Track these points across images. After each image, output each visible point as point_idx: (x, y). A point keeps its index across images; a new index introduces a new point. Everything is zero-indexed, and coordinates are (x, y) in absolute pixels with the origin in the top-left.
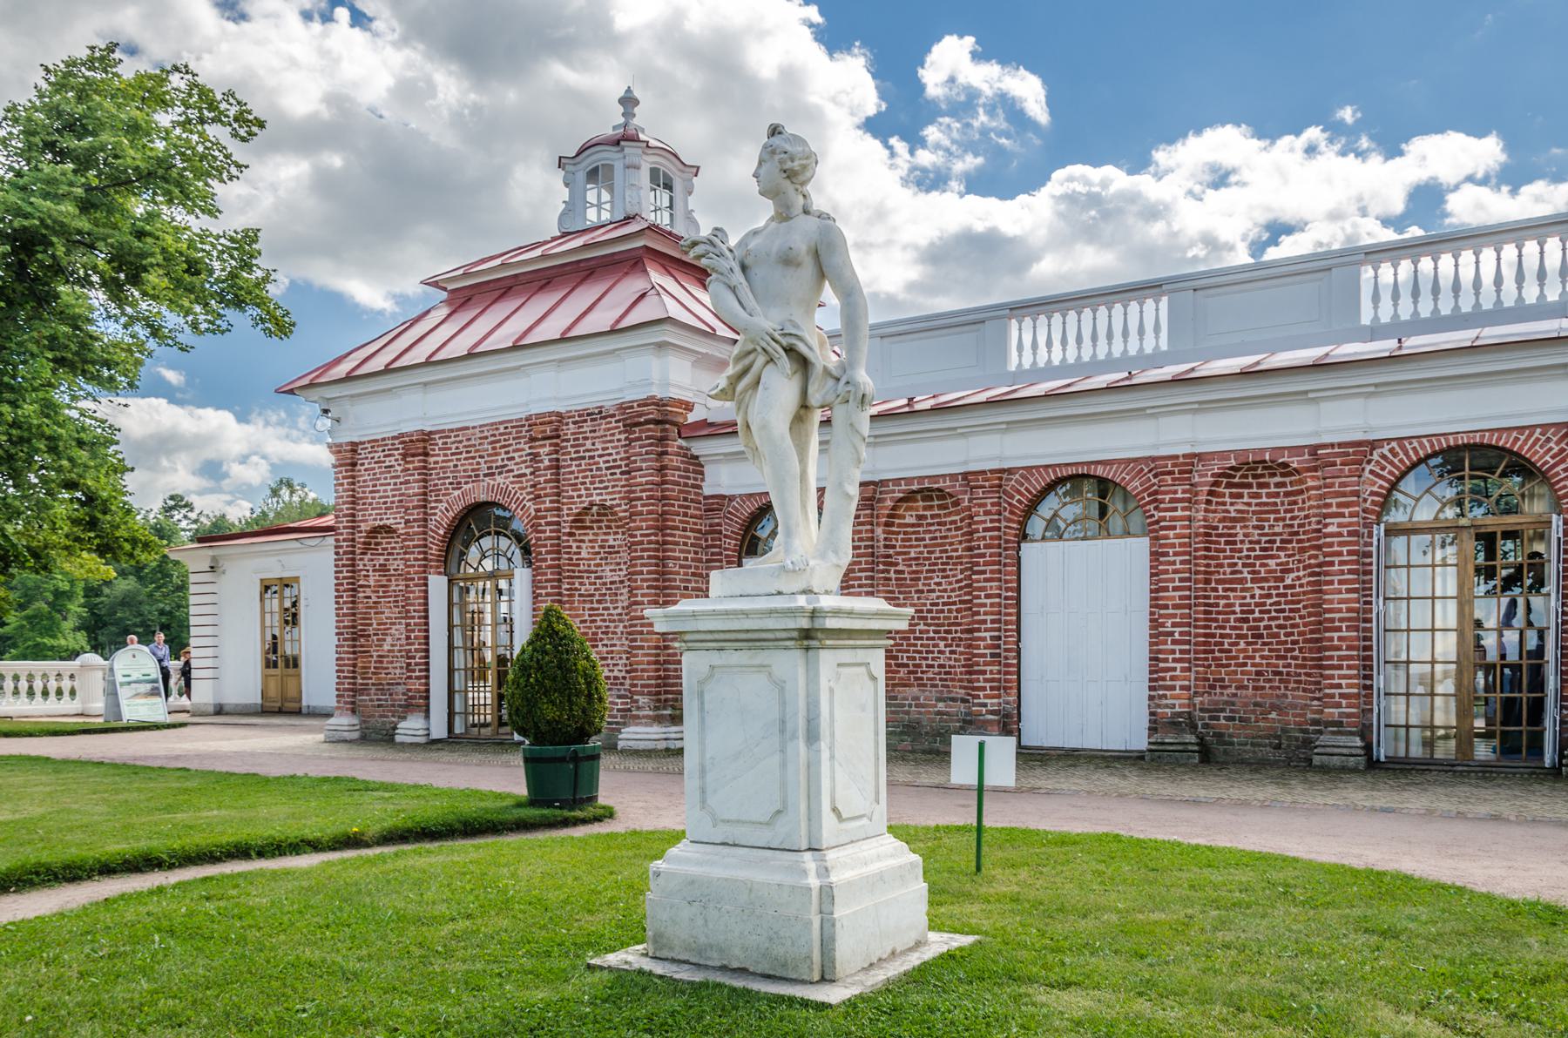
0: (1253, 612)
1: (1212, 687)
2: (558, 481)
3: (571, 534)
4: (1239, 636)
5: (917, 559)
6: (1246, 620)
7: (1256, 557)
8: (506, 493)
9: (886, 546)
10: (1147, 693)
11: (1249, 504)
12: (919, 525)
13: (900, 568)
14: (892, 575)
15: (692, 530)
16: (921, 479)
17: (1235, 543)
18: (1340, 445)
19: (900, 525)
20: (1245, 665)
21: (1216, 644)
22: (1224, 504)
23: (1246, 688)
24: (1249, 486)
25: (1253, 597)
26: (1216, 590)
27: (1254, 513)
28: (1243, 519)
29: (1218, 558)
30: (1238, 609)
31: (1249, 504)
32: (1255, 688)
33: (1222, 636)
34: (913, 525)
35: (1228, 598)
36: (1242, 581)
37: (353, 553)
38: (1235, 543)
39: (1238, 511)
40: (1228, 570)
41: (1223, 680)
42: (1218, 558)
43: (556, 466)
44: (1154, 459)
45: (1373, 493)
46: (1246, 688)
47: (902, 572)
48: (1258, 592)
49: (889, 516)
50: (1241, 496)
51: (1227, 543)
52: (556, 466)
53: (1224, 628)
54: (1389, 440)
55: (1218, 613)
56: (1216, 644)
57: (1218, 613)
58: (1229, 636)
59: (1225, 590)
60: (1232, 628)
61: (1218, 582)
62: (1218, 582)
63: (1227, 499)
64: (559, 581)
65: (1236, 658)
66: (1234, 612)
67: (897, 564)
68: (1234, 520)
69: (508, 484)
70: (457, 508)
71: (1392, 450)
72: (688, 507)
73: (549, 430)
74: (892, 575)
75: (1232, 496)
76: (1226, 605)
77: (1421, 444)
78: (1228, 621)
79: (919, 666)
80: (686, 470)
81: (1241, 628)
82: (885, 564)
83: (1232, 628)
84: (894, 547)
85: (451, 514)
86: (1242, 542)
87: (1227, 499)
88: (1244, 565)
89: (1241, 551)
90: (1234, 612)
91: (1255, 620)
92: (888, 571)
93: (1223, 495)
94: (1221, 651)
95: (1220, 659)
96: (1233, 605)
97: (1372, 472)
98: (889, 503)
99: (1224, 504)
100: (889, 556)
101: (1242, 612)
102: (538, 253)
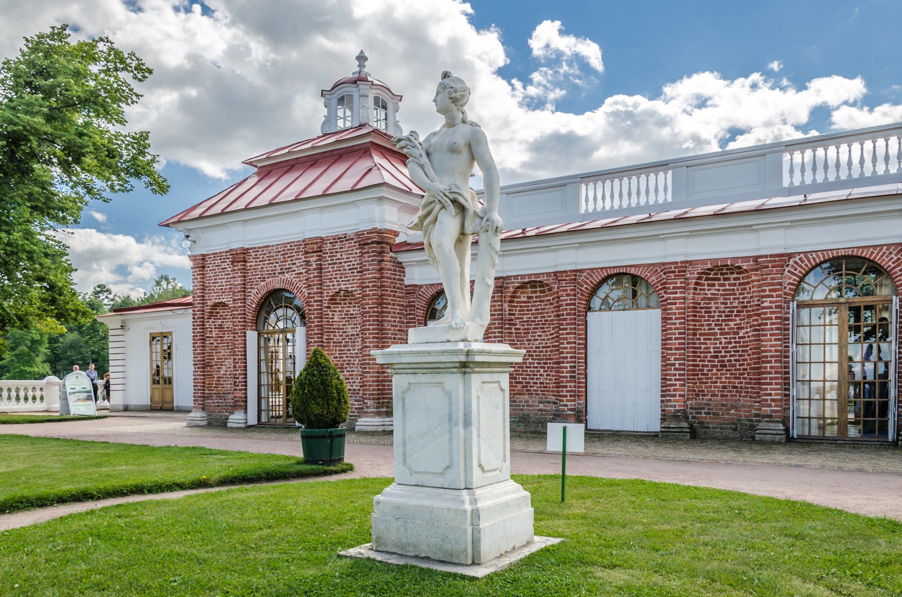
0: (721, 352)
1: (697, 395)
2: (321, 277)
3: (328, 307)
4: (713, 366)
5: (527, 321)
6: (717, 357)
7: (723, 321)
8: (291, 283)
9: (510, 314)
10: (660, 398)
11: (719, 290)
12: (529, 302)
13: (518, 327)
14: (513, 331)
15: (398, 305)
16: (530, 275)
17: (710, 312)
18: (771, 256)
19: (518, 302)
20: (716, 382)
21: (699, 370)
22: (704, 290)
23: (717, 395)
24: (719, 279)
25: (721, 343)
26: (699, 339)
27: (721, 295)
28: (715, 299)
29: (700, 321)
30: (712, 350)
31: (719, 290)
32: (722, 396)
33: (703, 366)
34: (525, 302)
35: (706, 344)
36: (715, 334)
37: (203, 318)
38: (710, 312)
39: (712, 294)
40: (707, 328)
41: (703, 391)
42: (700, 321)
43: (320, 268)
44: (664, 264)
45: (790, 284)
46: (717, 395)
47: (519, 329)
48: (723, 340)
49: (512, 297)
50: (714, 285)
51: (706, 312)
52: (320, 268)
53: (704, 361)
54: (799, 253)
55: (701, 352)
56: (699, 370)
57: (701, 352)
58: (707, 366)
59: (705, 339)
60: (709, 361)
61: (701, 335)
62: (701, 335)
63: (706, 287)
64: (322, 334)
65: (711, 378)
66: (710, 352)
67: (516, 325)
68: (710, 299)
69: (292, 278)
70: (263, 292)
71: (801, 259)
72: (396, 292)
73: (316, 247)
74: (513, 331)
75: (709, 285)
76: (705, 348)
77: (818, 255)
78: (706, 357)
79: (529, 383)
80: (395, 270)
81: (714, 361)
82: (509, 324)
83: (709, 361)
84: (514, 314)
85: (259, 296)
86: (715, 312)
87: (706, 287)
88: (716, 325)
89: (714, 317)
90: (710, 352)
91: (722, 357)
92: (511, 329)
93: (704, 285)
94: (702, 374)
95: (702, 379)
96: (709, 348)
97: (789, 271)
98: (512, 289)
99: (704, 290)
100: (512, 320)
101: (715, 352)
102: (309, 145)
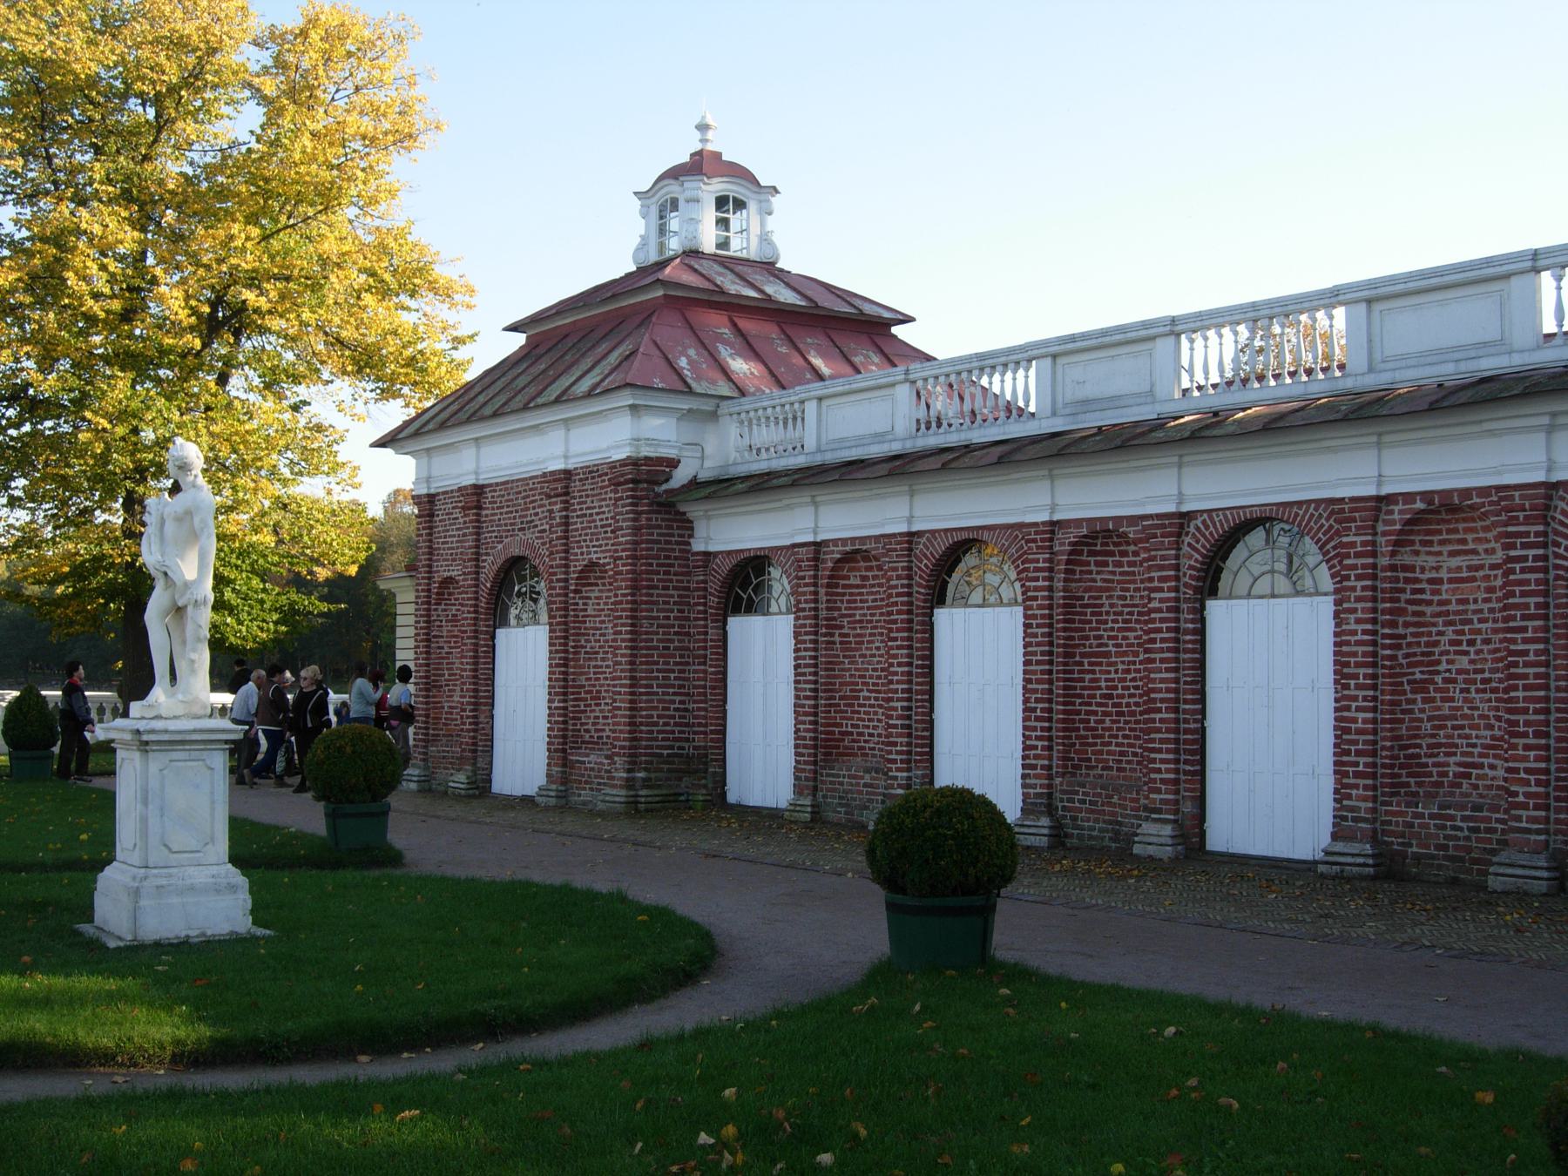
0: (1116, 688)
1: (1077, 767)
2: (567, 538)
3: (576, 592)
4: (1105, 714)
5: (861, 621)
6: (1110, 697)
7: (1119, 630)
8: (533, 548)
9: (828, 609)
10: (1020, 771)
11: (1113, 573)
12: (864, 586)
13: (845, 631)
14: (837, 639)
15: (675, 588)
16: (853, 540)
17: (1100, 614)
18: (1159, 516)
19: (845, 586)
20: (1110, 744)
21: (1081, 721)
22: (1090, 572)
23: (1111, 768)
24: (1112, 554)
25: (1116, 672)
26: (1081, 664)
27: (1119, 582)
28: (1108, 589)
29: (1083, 630)
30: (1103, 684)
31: (1113, 573)
32: (1119, 769)
33: (1088, 713)
34: (857, 586)
35: (1093, 672)
36: (1107, 655)
37: (429, 603)
38: (1100, 614)
39: (1104, 580)
40: (1095, 642)
41: (1089, 760)
42: (1083, 630)
43: (566, 523)
44: (1499, 488)
45: (1191, 567)
46: (1111, 768)
47: (847, 635)
48: (1121, 667)
49: (830, 577)
50: (1106, 564)
51: (1093, 614)
52: (566, 523)
53: (1090, 704)
54: (1203, 512)
55: (1083, 688)
56: (1081, 721)
57: (1083, 688)
58: (1095, 713)
59: (1090, 664)
60: (1099, 705)
61: (1083, 655)
62: (1083, 655)
63: (1093, 568)
64: (566, 638)
65: (1102, 736)
66: (1100, 688)
67: (842, 627)
68: (1101, 589)
69: (529, 538)
70: (500, 562)
71: (1204, 522)
72: (672, 565)
73: (562, 483)
74: (837, 639)
75: (1097, 564)
76: (1092, 680)
77: (1225, 516)
78: (1094, 696)
79: (862, 734)
80: (668, 527)
81: (1106, 705)
82: (827, 627)
83: (1099, 705)
84: (839, 609)
85: (495, 567)
86: (1108, 613)
87: (1093, 568)
88: (1110, 638)
89: (1106, 622)
90: (1100, 688)
91: (1119, 696)
92: (832, 635)
93: (1088, 563)
94: (1085, 729)
95: (1086, 737)
96: (1097, 680)
97: (1189, 545)
98: (830, 564)
99: (1090, 572)
100: (834, 619)
101: (1108, 688)
102: (1486, 426)
